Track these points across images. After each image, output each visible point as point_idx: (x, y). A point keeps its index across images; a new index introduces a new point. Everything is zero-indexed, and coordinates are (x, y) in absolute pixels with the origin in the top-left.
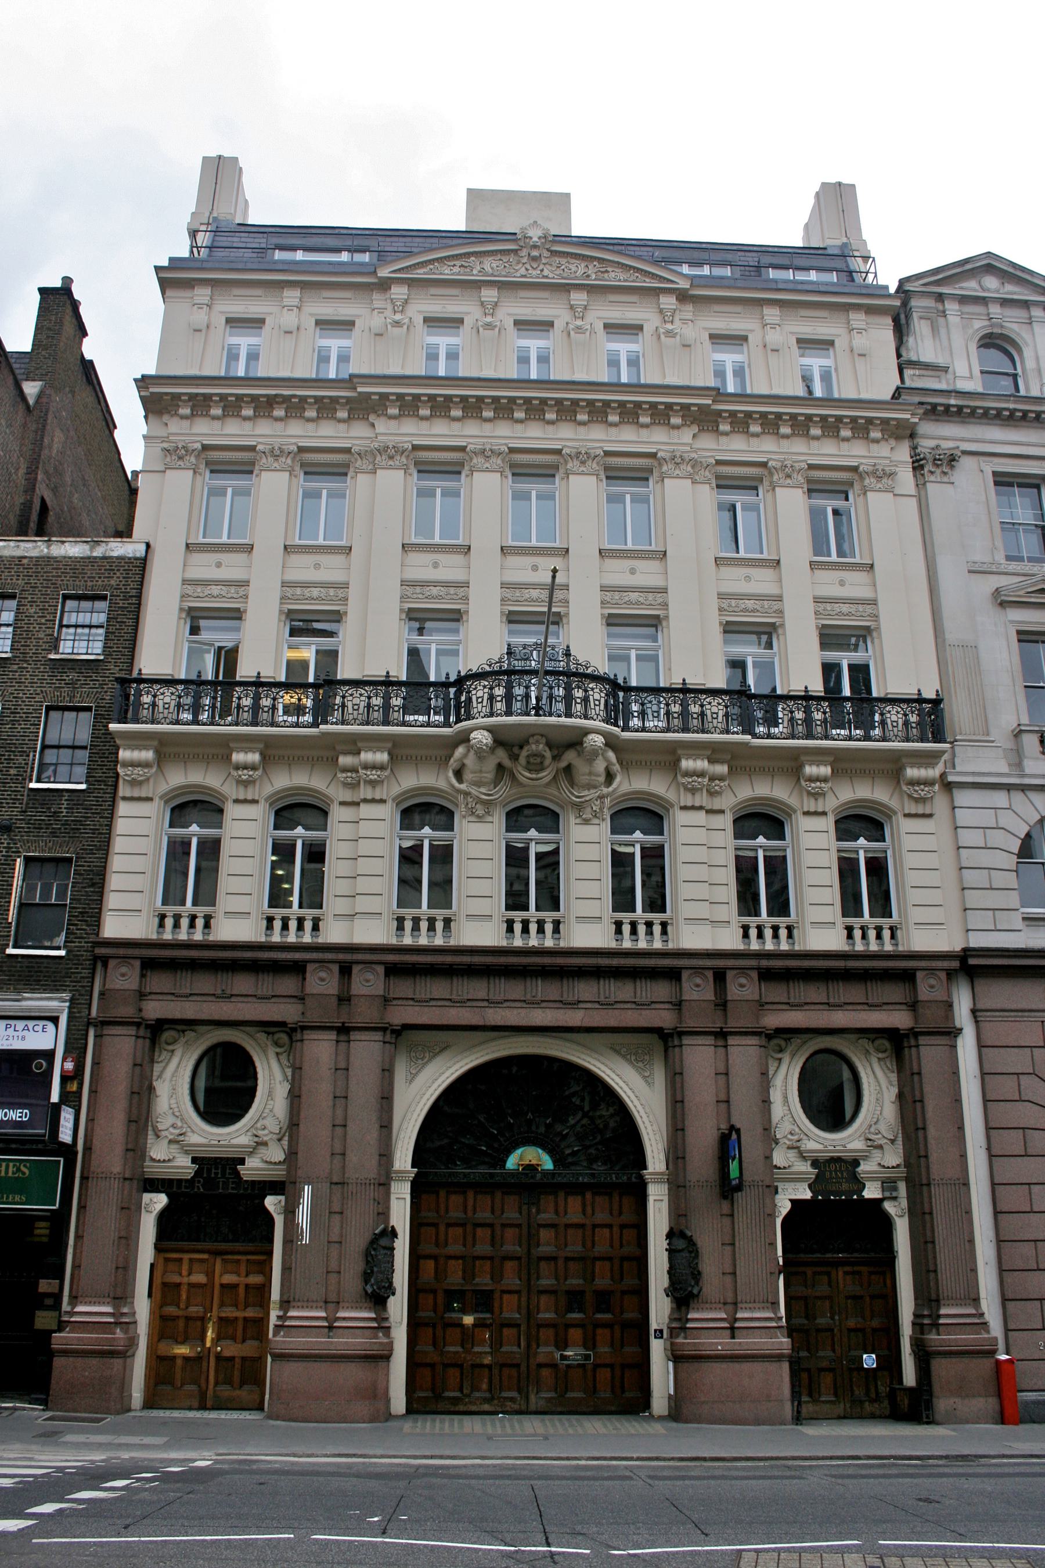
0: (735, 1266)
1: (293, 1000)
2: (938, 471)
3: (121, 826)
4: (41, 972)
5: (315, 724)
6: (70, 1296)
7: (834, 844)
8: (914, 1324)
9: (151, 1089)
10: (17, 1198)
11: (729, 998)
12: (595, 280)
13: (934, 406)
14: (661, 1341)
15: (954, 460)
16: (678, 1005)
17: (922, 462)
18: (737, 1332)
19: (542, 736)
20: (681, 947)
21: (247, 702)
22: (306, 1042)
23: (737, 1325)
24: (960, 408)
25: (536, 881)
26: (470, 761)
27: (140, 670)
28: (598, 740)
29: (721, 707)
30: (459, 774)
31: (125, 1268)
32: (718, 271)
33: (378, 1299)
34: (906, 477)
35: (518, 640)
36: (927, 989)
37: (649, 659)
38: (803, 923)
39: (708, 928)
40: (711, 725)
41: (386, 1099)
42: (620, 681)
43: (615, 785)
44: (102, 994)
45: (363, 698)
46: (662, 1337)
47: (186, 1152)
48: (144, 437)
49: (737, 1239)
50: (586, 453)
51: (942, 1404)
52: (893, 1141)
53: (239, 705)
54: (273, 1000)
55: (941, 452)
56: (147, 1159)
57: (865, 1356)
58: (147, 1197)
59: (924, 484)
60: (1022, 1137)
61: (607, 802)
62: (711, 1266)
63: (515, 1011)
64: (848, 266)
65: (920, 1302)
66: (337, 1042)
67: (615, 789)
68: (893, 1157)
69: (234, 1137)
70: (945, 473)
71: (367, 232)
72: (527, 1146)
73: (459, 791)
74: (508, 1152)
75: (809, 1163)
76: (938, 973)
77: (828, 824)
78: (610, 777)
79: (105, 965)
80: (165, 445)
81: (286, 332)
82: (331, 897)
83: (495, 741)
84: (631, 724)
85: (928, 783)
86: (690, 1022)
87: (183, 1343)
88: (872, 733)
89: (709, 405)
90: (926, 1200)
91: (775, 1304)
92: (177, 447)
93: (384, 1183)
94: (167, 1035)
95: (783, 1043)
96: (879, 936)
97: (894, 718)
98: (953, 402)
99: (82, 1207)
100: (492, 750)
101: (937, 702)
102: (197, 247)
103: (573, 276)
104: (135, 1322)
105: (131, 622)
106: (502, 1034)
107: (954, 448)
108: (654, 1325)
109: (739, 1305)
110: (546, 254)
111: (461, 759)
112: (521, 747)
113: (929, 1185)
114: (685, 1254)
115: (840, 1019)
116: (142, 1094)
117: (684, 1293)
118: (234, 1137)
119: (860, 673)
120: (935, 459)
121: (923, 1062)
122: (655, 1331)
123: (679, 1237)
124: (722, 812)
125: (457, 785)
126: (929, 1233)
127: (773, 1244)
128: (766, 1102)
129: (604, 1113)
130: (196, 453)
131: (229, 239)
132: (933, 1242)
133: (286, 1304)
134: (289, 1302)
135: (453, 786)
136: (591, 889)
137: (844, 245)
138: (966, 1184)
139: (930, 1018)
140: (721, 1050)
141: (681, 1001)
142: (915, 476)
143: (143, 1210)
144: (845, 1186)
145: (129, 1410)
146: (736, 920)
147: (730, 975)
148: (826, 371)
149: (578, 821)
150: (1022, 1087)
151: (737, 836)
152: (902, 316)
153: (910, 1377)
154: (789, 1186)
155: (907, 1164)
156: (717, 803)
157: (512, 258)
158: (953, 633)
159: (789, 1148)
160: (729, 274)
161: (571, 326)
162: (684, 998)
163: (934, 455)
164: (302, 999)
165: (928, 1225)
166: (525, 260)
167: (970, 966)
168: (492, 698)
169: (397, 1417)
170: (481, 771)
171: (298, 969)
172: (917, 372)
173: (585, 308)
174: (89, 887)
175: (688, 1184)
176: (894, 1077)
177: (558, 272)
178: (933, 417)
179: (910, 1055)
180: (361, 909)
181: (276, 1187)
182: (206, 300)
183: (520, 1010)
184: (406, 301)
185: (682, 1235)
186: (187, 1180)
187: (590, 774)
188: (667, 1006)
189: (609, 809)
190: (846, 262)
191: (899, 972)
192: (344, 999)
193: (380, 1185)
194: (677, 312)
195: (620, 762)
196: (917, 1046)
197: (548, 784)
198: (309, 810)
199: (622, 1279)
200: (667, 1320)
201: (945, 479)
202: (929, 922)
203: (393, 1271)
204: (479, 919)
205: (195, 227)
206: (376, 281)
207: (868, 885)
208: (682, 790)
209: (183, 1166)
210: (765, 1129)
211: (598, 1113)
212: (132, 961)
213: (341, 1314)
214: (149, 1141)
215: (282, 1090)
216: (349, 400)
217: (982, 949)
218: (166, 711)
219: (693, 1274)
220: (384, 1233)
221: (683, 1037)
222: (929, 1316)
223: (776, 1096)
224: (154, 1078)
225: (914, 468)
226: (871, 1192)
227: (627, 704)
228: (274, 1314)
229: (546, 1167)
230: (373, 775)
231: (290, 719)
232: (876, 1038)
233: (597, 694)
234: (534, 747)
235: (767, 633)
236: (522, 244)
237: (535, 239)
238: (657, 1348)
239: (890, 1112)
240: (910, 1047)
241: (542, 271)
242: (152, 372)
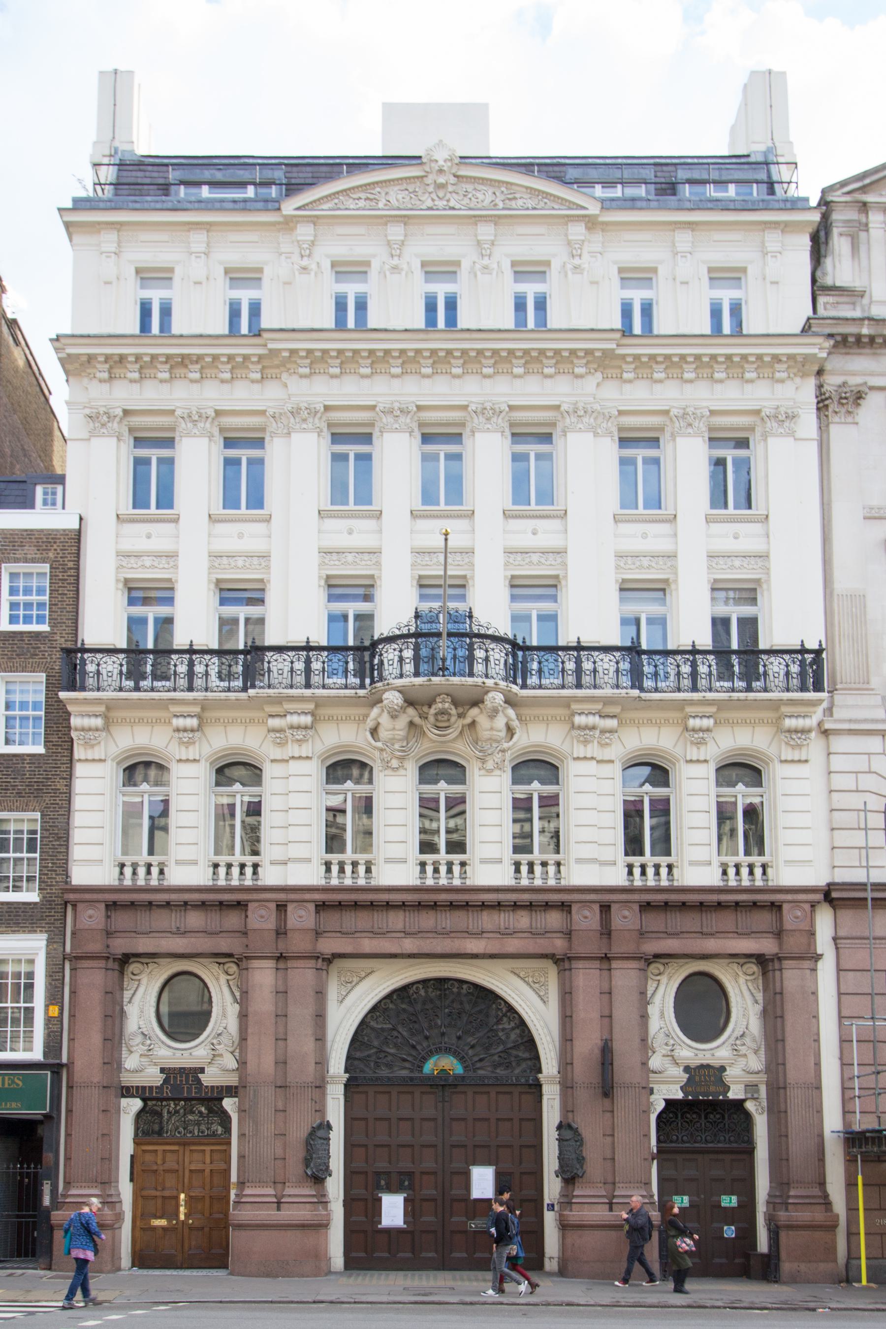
0: (614, 1153)
1: (237, 935)
2: (843, 410)
3: (79, 785)
4: (20, 916)
5: (245, 689)
6: (64, 1182)
7: (713, 790)
8: (768, 1202)
9: (122, 1012)
10: (14, 1105)
11: (613, 928)
12: (504, 209)
13: (845, 337)
14: (552, 1213)
15: (860, 398)
16: (568, 934)
17: (826, 402)
18: (614, 1206)
19: (448, 695)
20: (571, 884)
21: (182, 669)
22: (250, 970)
23: (614, 1201)
24: (872, 339)
25: (444, 829)
26: (385, 720)
27: (83, 641)
28: (499, 698)
29: (611, 663)
30: (374, 732)
31: (110, 1160)
32: (631, 191)
33: (318, 1179)
34: (809, 421)
35: (425, 606)
36: (791, 917)
37: (549, 619)
38: (682, 861)
39: (596, 867)
40: (602, 681)
41: (320, 1017)
42: (520, 641)
43: (515, 738)
44: (73, 933)
45: (286, 663)
46: (553, 1210)
47: (155, 1064)
48: (67, 403)
49: (616, 1131)
50: (492, 409)
51: (786, 1267)
52: (756, 1052)
53: (175, 671)
54: (221, 935)
55: (848, 389)
56: (123, 1070)
57: (725, 1228)
58: (124, 1102)
59: (828, 426)
60: (872, 1048)
61: (508, 755)
62: (593, 1152)
63: (428, 941)
64: (769, 176)
65: (773, 1185)
66: (277, 969)
67: (515, 743)
68: (756, 1063)
69: (716, 1052)
70: (849, 412)
71: (273, 161)
72: (443, 1068)
73: (375, 748)
74: (424, 1060)
75: (682, 1068)
76: (802, 905)
77: (709, 771)
78: (510, 731)
79: (74, 906)
80: (87, 411)
81: (195, 283)
82: (267, 845)
83: (406, 701)
84: (529, 682)
85: (805, 731)
86: (580, 949)
87: (161, 1218)
88: (754, 684)
89: (613, 350)
90: (782, 1100)
91: (648, 1184)
92: (99, 413)
93: (320, 1086)
94: (133, 967)
95: (661, 968)
96: (657, 873)
97: (776, 669)
98: (865, 331)
99: (69, 1111)
100: (403, 709)
101: (818, 652)
102: (100, 184)
103: (479, 206)
104: (121, 1202)
105: (71, 594)
106: (418, 960)
107: (861, 385)
108: (547, 1201)
109: (617, 1185)
110: (453, 180)
111: (376, 719)
112: (430, 707)
113: (785, 1088)
114: (572, 1143)
115: (711, 945)
116: (114, 1017)
117: (570, 1176)
118: (192, 1053)
119: (749, 625)
120: (841, 398)
121: (785, 983)
122: (548, 1205)
123: (567, 1130)
124: (612, 762)
125: (373, 742)
126: (783, 1129)
127: (647, 1136)
128: (644, 1017)
129: (507, 1026)
130: (117, 419)
131: (134, 174)
132: (787, 1136)
133: (241, 1184)
134: (244, 1183)
135: (370, 744)
136: (492, 834)
137: (770, 150)
138: (819, 1088)
139: (793, 944)
140: (606, 973)
141: (571, 931)
142: (819, 418)
143: (122, 1112)
144: (712, 1089)
145: (119, 1269)
146: (622, 860)
147: (614, 908)
148: (736, 304)
149: (483, 772)
150: (875, 1006)
151: (719, 784)
152: (822, 234)
153: (763, 1244)
154: (664, 1087)
155: (768, 1070)
156: (607, 753)
157: (417, 186)
158: (841, 584)
159: (664, 1056)
160: (644, 195)
161: (478, 266)
162: (573, 928)
163: (840, 394)
164: (245, 934)
165: (783, 1121)
166: (431, 189)
167: (831, 896)
168: (401, 659)
169: (336, 1273)
170: (394, 729)
171: (240, 906)
172: (836, 299)
173: (493, 244)
174: (56, 840)
175: (575, 1085)
176: (760, 996)
177: (464, 203)
178: (843, 351)
179: (774, 977)
180: (293, 857)
181: (231, 1091)
182: (112, 247)
183: (432, 940)
184: (313, 243)
185: (569, 1126)
186: (157, 1087)
187: (492, 729)
188: (559, 935)
189: (510, 761)
190: (769, 171)
191: (763, 906)
192: (281, 932)
193: (316, 1087)
194: (586, 244)
195: (519, 717)
196: (781, 970)
197: (455, 739)
198: (235, 767)
199: (521, 1163)
200: (558, 1196)
201: (850, 419)
202: (799, 857)
203: (330, 1157)
204: (396, 863)
205: (97, 161)
206: (281, 219)
207: (748, 827)
208: (689, 743)
209: (153, 1077)
210: (643, 1040)
211: (501, 1027)
212: (97, 905)
213: (792, 1193)
214: (123, 1056)
215: (233, 1010)
216: (260, 357)
217: (844, 884)
218: (110, 679)
219: (578, 1159)
220: (320, 1126)
221: (573, 962)
222: (781, 1196)
223: (653, 1011)
224: (125, 1003)
225: (818, 409)
226: (735, 1093)
227: (524, 663)
228: (233, 1193)
229: (457, 1072)
230: (299, 735)
231: (222, 684)
232: (745, 963)
233: (498, 654)
234: (440, 705)
235: (660, 589)
236: (428, 169)
237: (441, 163)
238: (550, 1219)
239: (755, 1026)
240: (774, 970)
241: (448, 201)
242: (68, 331)
